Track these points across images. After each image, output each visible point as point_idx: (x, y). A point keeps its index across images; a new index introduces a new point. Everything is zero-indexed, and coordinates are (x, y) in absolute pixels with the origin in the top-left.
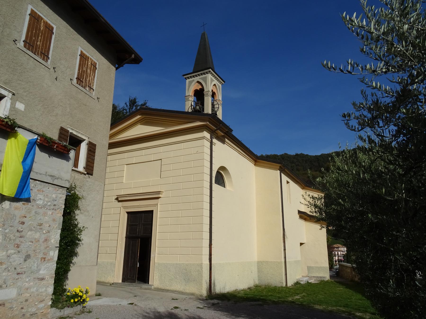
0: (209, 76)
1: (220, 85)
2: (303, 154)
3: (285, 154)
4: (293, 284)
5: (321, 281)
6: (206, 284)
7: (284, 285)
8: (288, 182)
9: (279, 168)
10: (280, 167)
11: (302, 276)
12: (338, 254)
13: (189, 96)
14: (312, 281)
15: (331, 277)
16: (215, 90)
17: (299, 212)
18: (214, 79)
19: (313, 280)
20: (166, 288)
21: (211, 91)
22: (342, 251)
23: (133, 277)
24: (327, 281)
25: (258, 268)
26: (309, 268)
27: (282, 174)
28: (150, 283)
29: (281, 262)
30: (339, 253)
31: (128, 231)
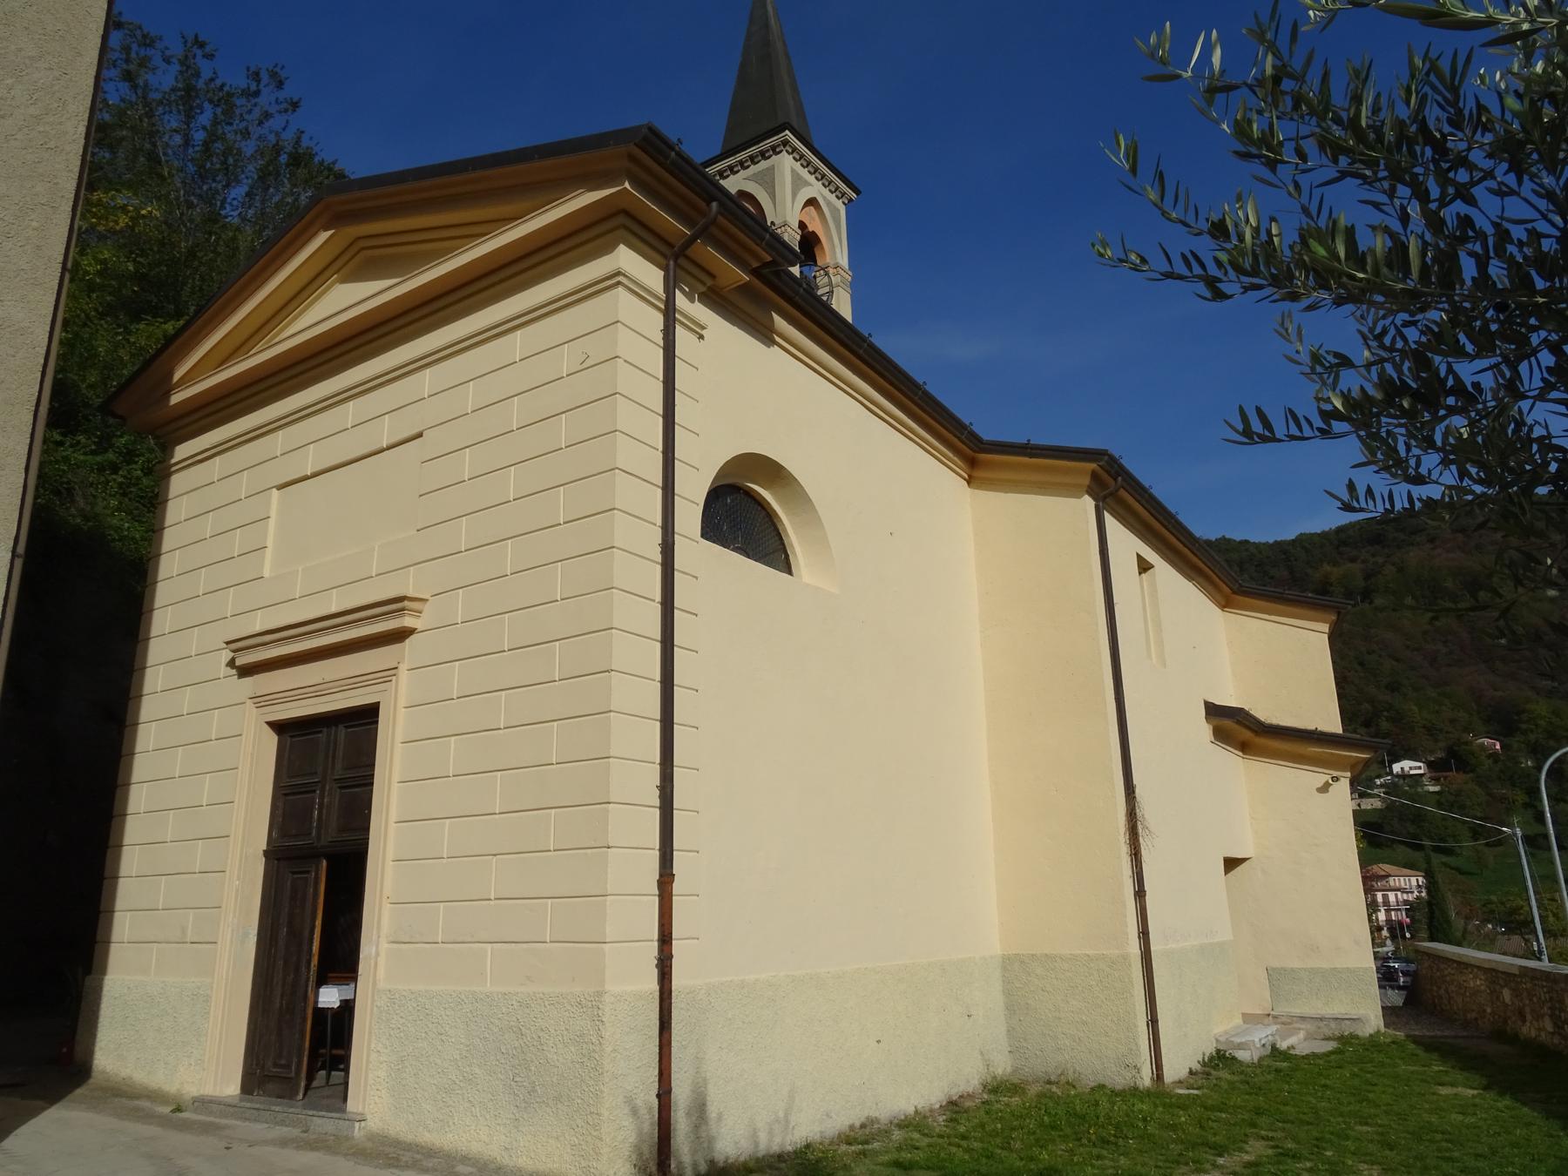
0: (785, 164)
1: (839, 204)
4: (1196, 1067)
5: (1341, 1039)
6: (627, 1122)
7: (1146, 1079)
8: (1144, 566)
9: (1087, 481)
10: (1095, 476)
11: (1247, 1018)
12: (1386, 902)
14: (1298, 1042)
15: (1388, 1011)
16: (814, 226)
17: (1213, 711)
18: (811, 179)
19: (1302, 1035)
20: (419, 1140)
21: (796, 225)
22: (1403, 891)
23: (288, 1066)
24: (1373, 1043)
25: (1007, 993)
26: (1277, 977)
27: (1109, 519)
28: (352, 1105)
29: (1125, 957)
30: (1392, 897)
31: (280, 812)
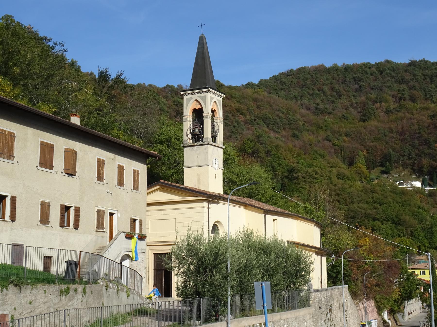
2: (426, 62)
3: (388, 61)
13: (187, 116)
